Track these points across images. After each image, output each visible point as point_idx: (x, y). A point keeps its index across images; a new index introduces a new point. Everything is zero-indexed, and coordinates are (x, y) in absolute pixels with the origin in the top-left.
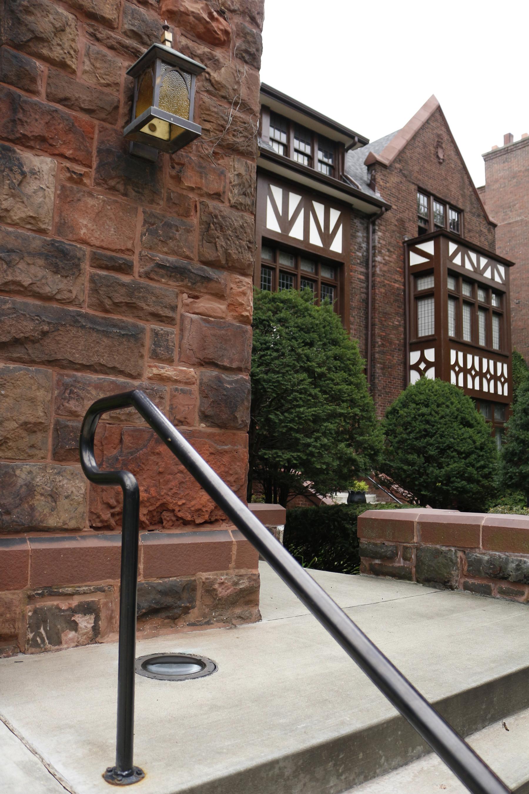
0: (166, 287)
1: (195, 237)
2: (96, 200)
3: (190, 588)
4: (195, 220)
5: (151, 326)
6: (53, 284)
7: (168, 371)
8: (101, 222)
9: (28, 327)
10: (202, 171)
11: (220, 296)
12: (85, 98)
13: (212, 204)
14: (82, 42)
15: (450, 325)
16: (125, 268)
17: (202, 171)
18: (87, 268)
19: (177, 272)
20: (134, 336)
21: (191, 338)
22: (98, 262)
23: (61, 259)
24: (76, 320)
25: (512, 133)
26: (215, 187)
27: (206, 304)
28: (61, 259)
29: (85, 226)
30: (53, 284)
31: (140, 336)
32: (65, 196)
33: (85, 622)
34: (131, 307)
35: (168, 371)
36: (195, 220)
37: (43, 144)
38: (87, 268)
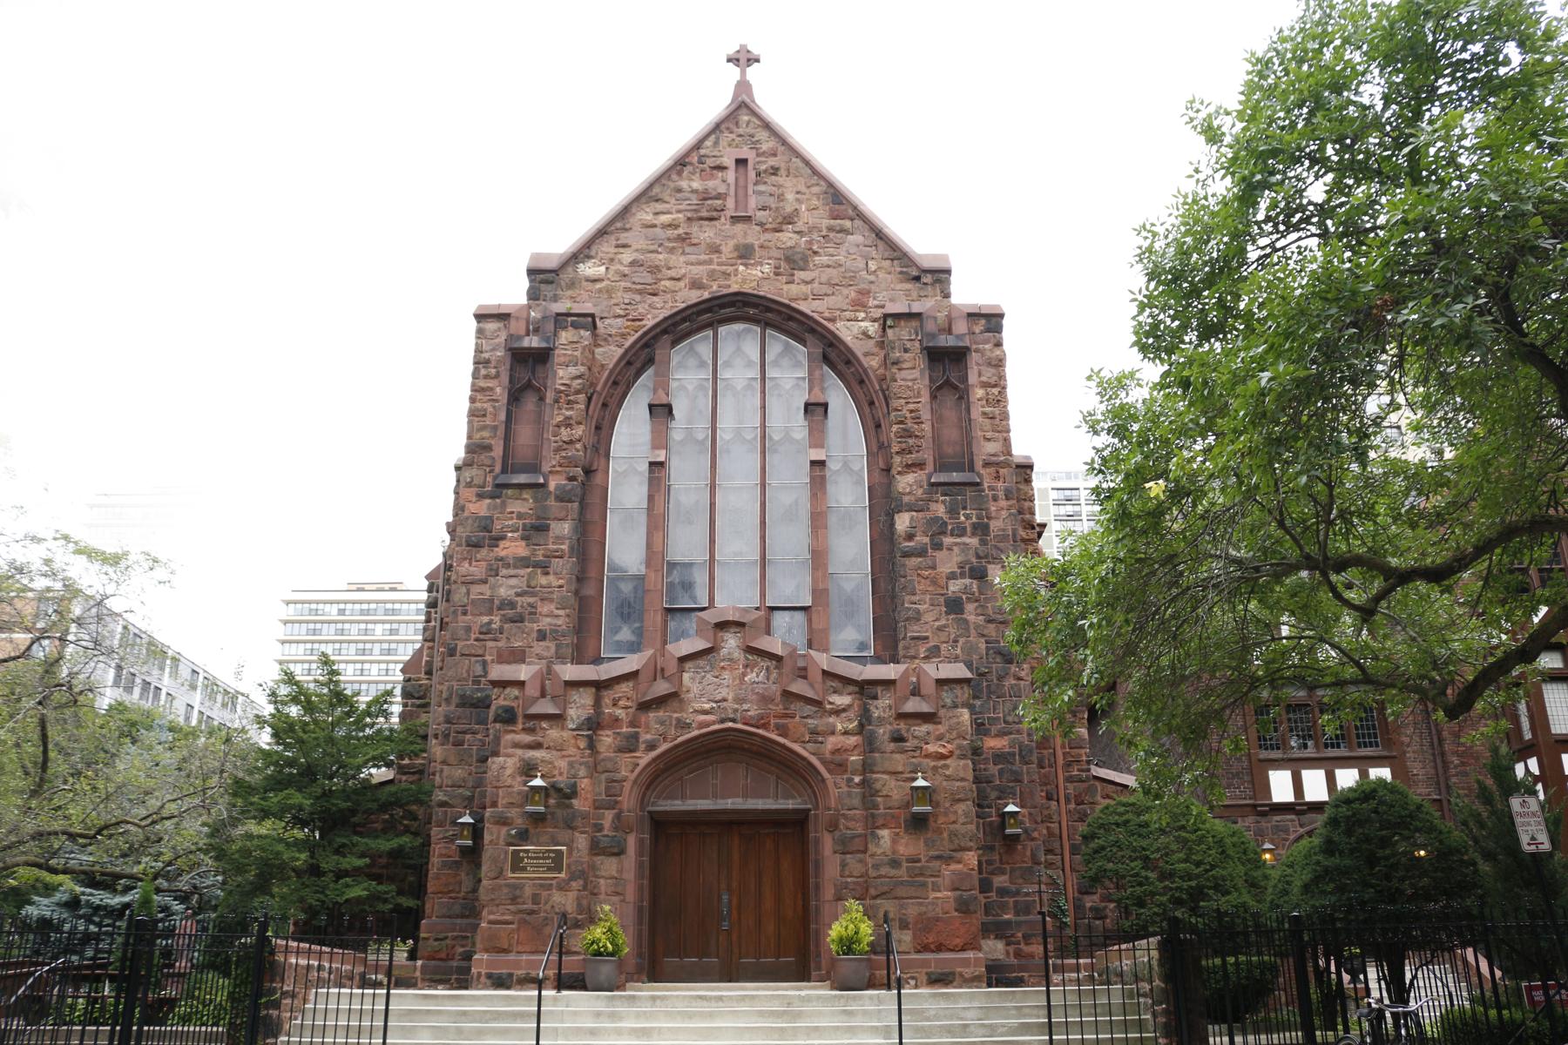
0: (936, 864)
1: (946, 843)
2: (905, 839)
3: (953, 974)
4: (945, 835)
5: (930, 880)
6: (893, 872)
7: (939, 895)
8: (908, 847)
9: (886, 889)
10: (946, 814)
11: (959, 862)
12: (896, 804)
13: (952, 827)
14: (893, 783)
15: (760, 807)
16: (919, 861)
17: (946, 814)
18: (905, 864)
19: (938, 858)
20: (924, 885)
21: (947, 881)
22: (908, 861)
23: (895, 863)
24: (902, 883)
25: (473, 310)
26: (953, 818)
27: (954, 867)
28: (895, 863)
29: (901, 849)
30: (893, 872)
31: (212, 881)
32: (894, 841)
33: (912, 982)
34: (922, 875)
35: (939, 895)
36: (945, 835)
37: (884, 826)
38: (905, 864)
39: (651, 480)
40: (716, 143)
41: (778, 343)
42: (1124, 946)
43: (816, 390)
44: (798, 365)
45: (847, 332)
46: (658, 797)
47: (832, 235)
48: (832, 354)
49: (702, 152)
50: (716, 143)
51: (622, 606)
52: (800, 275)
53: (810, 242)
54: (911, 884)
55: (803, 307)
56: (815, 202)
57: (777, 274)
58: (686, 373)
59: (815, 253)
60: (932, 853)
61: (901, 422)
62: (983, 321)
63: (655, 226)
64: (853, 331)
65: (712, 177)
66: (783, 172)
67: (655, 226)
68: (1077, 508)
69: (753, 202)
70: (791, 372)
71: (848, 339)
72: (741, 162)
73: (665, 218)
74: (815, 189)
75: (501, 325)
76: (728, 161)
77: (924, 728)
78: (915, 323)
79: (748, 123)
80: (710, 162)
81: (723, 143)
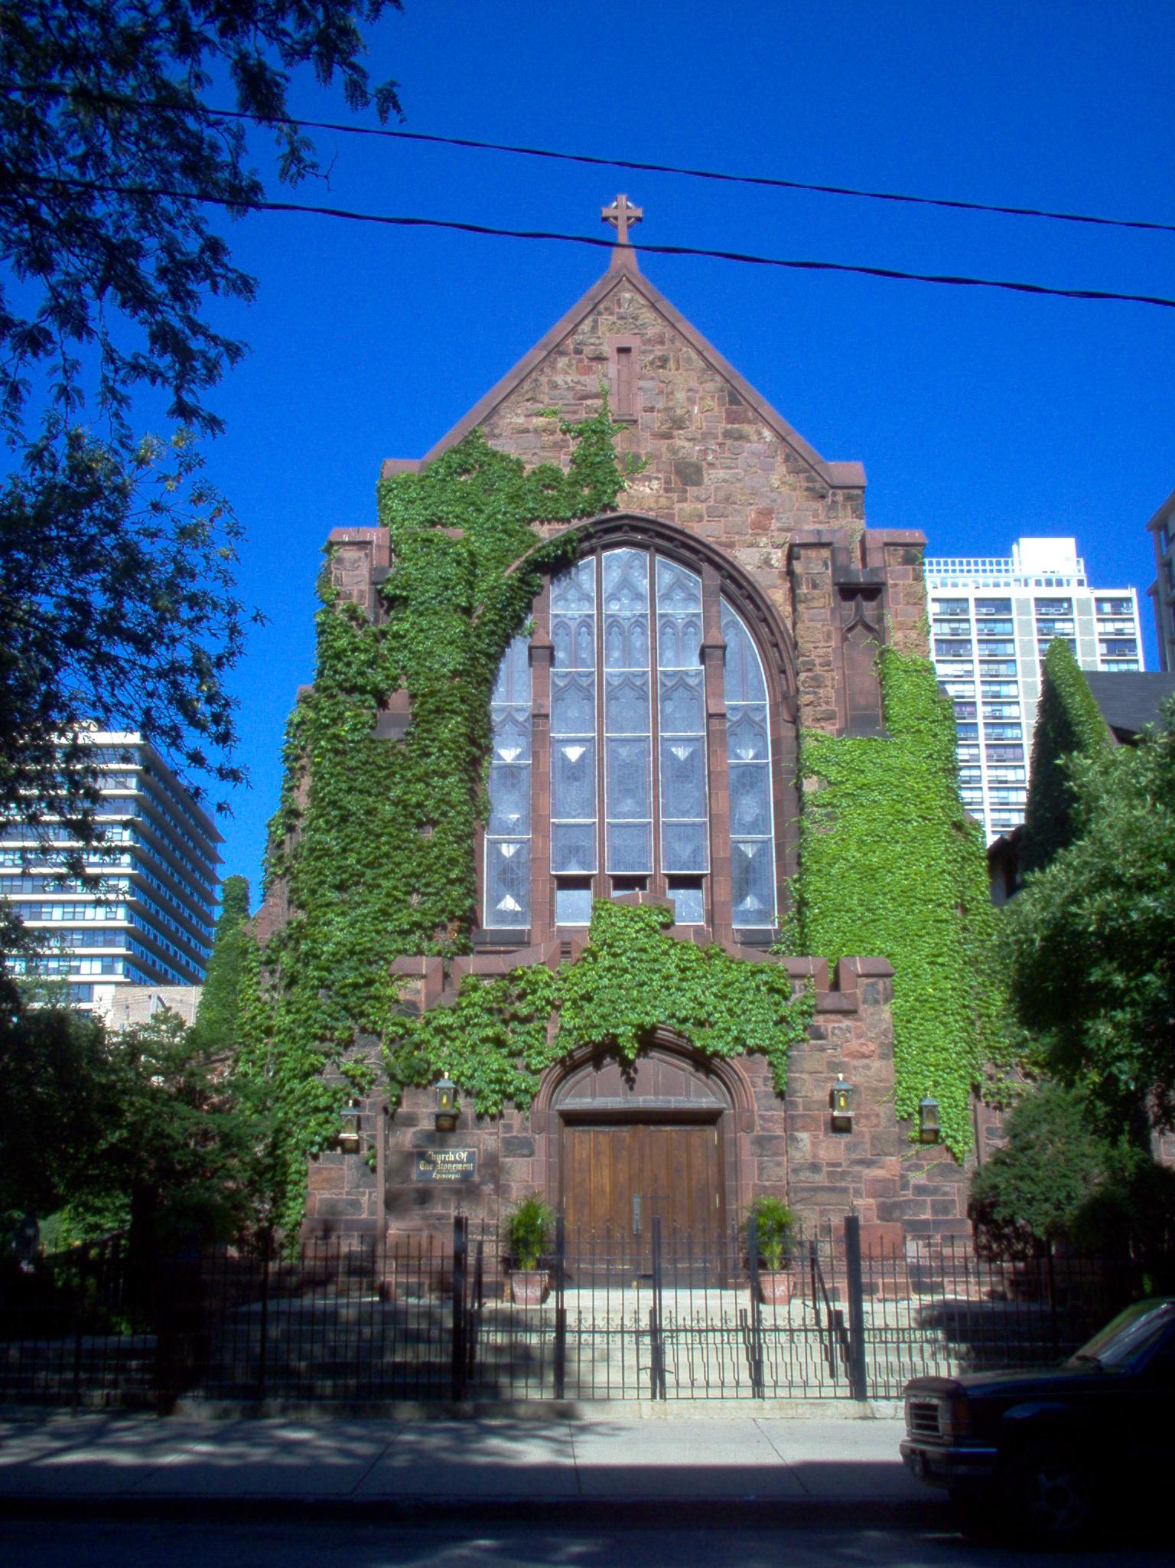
5: (852, 1185)
16: (839, 1165)
18: (825, 1169)
23: (815, 1167)
32: (813, 1144)
37: (804, 1129)
39: (535, 734)
40: (594, 328)
41: (668, 572)
42: (682, 1303)
43: (714, 631)
44: (691, 598)
45: (746, 559)
46: (567, 1095)
47: (729, 442)
48: (738, 589)
49: (579, 337)
50: (594, 328)
51: (504, 872)
52: (692, 491)
53: (705, 452)
54: (832, 1189)
55: (697, 530)
56: (709, 402)
57: (667, 490)
58: (564, 605)
59: (711, 465)
60: (854, 1156)
61: (809, 670)
62: (901, 551)
63: (527, 431)
64: (758, 559)
65: (588, 370)
66: (671, 364)
67: (527, 431)
68: (968, 667)
69: (641, 402)
70: (684, 598)
71: (749, 569)
72: (624, 351)
73: (540, 421)
74: (710, 386)
75: (362, 554)
76: (608, 350)
77: (847, 1023)
78: (825, 553)
79: (631, 301)
80: (588, 351)
81: (602, 329)
